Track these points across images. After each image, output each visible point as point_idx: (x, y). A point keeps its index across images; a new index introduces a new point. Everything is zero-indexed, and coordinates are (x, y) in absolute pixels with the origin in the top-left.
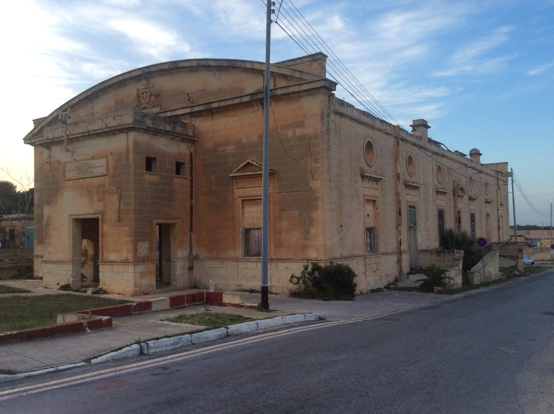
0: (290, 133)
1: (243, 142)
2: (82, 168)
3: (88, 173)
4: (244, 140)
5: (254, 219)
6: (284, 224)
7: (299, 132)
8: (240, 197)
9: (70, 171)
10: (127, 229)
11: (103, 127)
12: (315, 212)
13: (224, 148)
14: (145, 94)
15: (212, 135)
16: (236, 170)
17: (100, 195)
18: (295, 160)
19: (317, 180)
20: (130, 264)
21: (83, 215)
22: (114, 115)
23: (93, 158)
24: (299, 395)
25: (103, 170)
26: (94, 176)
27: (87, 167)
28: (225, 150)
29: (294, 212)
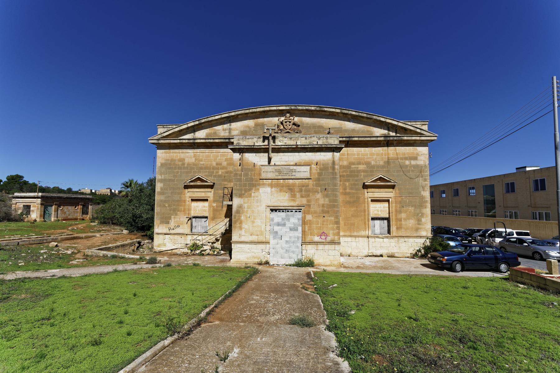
0: (407, 162)
1: (372, 164)
2: (282, 171)
3: (289, 175)
4: (373, 163)
5: (378, 212)
6: (403, 215)
7: (413, 162)
8: (370, 198)
9: (267, 172)
10: (333, 218)
11: (306, 143)
12: (425, 209)
13: (357, 166)
14: (288, 123)
15: (346, 156)
16: (371, 181)
17: (303, 193)
18: (411, 178)
19: (426, 191)
20: (336, 244)
21: (283, 206)
22: (319, 136)
23: (296, 165)
24: (345, 317)
25: (307, 175)
26: (296, 178)
27: (288, 171)
28: (358, 168)
29: (410, 208)
